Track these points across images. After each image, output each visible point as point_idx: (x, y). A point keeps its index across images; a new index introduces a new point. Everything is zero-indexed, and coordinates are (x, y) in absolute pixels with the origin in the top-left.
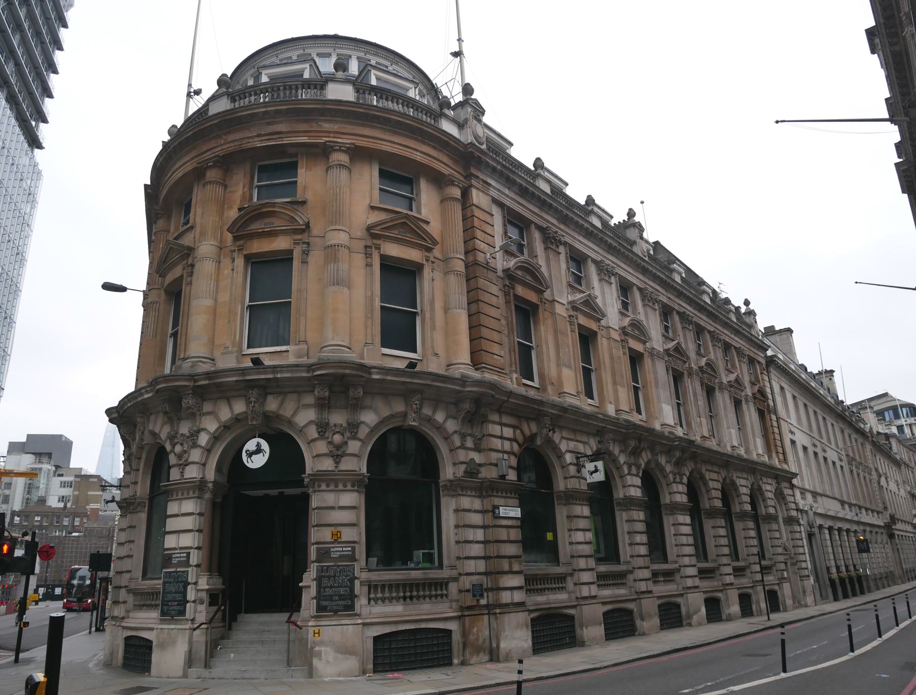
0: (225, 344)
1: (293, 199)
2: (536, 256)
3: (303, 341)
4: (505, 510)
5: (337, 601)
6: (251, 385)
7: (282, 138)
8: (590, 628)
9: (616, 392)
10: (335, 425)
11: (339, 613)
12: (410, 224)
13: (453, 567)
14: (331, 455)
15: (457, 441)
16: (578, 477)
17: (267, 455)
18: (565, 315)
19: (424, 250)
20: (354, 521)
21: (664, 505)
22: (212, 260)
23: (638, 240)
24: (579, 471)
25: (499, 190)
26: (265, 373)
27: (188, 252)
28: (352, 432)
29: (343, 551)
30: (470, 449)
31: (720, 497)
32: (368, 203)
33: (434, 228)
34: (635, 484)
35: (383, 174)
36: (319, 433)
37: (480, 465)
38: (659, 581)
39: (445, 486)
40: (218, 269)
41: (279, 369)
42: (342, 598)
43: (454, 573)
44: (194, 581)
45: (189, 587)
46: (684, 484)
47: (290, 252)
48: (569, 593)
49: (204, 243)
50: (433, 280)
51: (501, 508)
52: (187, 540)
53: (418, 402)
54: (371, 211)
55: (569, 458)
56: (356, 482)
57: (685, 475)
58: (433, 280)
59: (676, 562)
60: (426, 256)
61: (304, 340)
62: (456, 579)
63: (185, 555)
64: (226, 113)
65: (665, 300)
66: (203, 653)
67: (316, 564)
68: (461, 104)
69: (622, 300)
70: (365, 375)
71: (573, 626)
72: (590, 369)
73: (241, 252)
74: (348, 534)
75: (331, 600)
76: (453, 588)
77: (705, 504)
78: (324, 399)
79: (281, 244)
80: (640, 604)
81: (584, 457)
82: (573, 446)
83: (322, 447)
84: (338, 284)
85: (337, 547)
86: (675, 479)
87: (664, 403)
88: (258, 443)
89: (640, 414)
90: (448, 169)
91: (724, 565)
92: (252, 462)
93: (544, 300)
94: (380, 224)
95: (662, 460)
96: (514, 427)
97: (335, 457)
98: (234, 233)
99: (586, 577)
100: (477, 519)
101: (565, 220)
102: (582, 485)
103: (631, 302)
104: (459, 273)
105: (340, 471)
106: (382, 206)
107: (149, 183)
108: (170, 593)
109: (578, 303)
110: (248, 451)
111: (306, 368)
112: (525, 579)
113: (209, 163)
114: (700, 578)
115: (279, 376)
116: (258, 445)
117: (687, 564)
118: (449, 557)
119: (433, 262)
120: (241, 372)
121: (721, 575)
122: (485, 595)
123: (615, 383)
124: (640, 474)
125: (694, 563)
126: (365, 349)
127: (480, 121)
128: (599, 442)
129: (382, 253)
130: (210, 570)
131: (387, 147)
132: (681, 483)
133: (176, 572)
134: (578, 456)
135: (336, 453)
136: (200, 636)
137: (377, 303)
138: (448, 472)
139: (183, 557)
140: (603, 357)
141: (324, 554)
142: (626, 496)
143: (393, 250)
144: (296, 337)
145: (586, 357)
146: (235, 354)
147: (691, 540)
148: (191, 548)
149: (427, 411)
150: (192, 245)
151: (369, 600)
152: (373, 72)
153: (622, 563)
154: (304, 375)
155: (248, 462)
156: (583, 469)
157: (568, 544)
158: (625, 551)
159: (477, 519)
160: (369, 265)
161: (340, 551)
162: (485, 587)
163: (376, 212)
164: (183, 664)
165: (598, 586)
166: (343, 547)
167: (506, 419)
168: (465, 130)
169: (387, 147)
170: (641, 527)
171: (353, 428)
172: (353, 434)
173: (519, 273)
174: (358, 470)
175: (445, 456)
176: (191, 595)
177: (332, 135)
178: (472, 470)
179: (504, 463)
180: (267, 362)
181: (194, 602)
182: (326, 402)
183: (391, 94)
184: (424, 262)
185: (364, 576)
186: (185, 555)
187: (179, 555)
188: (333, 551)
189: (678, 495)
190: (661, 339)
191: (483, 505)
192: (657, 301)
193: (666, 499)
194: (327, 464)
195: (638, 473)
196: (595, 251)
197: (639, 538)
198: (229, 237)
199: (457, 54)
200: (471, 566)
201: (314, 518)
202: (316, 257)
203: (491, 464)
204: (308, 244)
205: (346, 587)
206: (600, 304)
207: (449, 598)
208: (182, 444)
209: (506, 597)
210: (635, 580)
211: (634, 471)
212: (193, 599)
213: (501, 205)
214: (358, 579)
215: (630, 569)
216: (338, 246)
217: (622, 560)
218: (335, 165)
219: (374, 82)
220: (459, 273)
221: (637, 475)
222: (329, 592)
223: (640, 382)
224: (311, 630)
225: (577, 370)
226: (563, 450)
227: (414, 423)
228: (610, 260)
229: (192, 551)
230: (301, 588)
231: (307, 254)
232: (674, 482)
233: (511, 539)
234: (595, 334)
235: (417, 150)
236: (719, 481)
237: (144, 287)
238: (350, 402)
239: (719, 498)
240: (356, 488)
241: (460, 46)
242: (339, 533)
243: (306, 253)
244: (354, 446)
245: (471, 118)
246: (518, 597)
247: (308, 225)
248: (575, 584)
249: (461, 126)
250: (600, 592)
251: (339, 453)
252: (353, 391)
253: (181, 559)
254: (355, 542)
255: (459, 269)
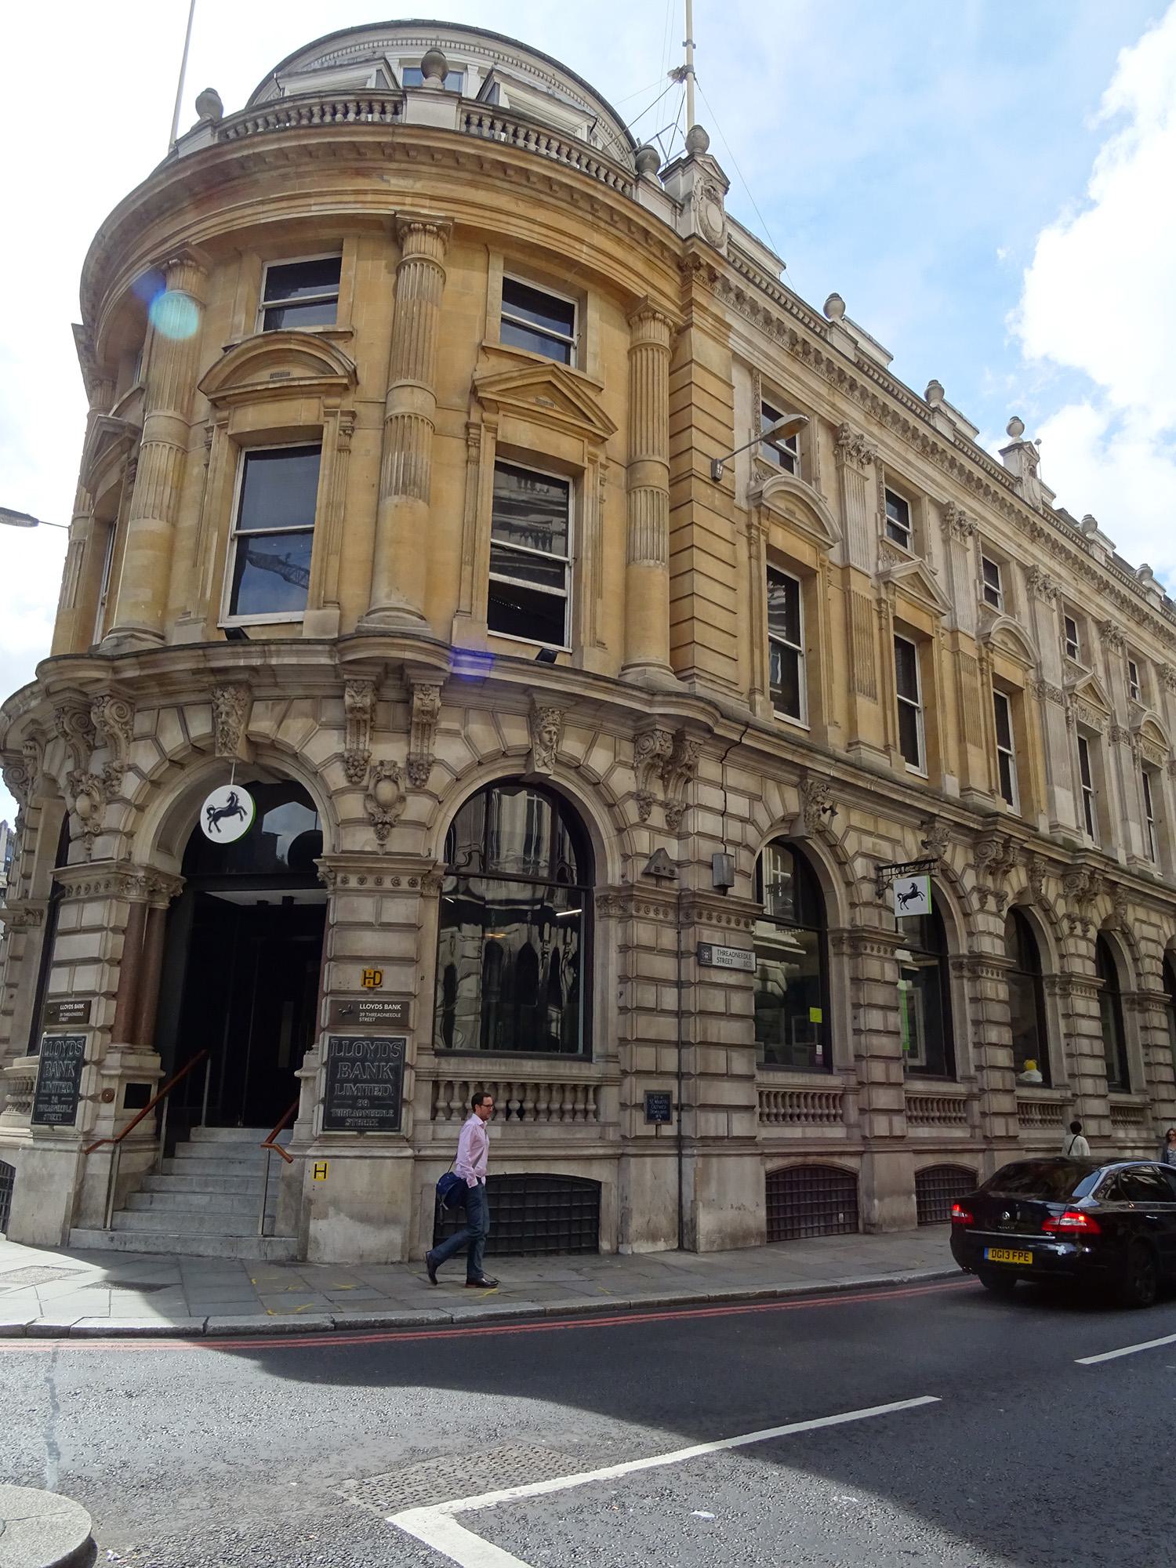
0: (185, 607)
1: (330, 328)
2: (817, 480)
3: (334, 602)
4: (724, 953)
5: (367, 1108)
6: (223, 678)
7: (310, 205)
8: (887, 1200)
9: (963, 755)
10: (382, 763)
11: (369, 1133)
12: (560, 386)
13: (613, 1058)
14: (371, 821)
15: (632, 810)
16: (879, 906)
17: (248, 819)
18: (869, 597)
19: (586, 441)
20: (412, 954)
21: (1048, 976)
22: (168, 446)
23: (1025, 476)
24: (880, 894)
25: (749, 342)
26: (247, 655)
27: (133, 437)
28: (416, 779)
29: (383, 1011)
30: (659, 831)
31: (1161, 973)
32: (477, 341)
33: (613, 403)
34: (992, 930)
35: (513, 293)
36: (350, 777)
37: (679, 864)
38: (1032, 1120)
39: (605, 899)
40: (182, 467)
41: (273, 648)
42: (376, 1102)
43: (613, 1069)
44: (95, 1058)
45: (85, 1070)
46: (1090, 940)
47: (317, 431)
48: (849, 1126)
49: (154, 413)
50: (602, 501)
51: (714, 949)
52: (87, 979)
53: (553, 729)
54: (482, 357)
55: (860, 867)
56: (424, 877)
57: (1092, 923)
58: (602, 501)
59: (1066, 1087)
60: (590, 453)
61: (334, 599)
62: (617, 1082)
63: (82, 1006)
64: (210, 153)
65: (1071, 593)
66: (102, 1200)
67: (328, 1035)
68: (680, 165)
69: (987, 588)
70: (444, 666)
71: (854, 1192)
72: (914, 708)
73: (224, 431)
74: (395, 979)
75: (353, 1107)
76: (610, 1098)
77: (1129, 982)
78: (362, 710)
79: (301, 412)
80: (992, 1158)
81: (891, 867)
82: (871, 846)
83: (353, 806)
84: (405, 492)
85: (373, 1003)
86: (1072, 929)
87: (1060, 785)
88: (232, 793)
89: (1010, 802)
90: (645, 286)
91: (1164, 1101)
92: (219, 830)
93: (827, 564)
94: (499, 382)
95: (1051, 889)
96: (755, 798)
97: (380, 826)
98: (212, 393)
99: (884, 1098)
100: (665, 967)
101: (881, 414)
102: (884, 922)
103: (1005, 592)
104: (655, 490)
105: (387, 854)
106: (504, 348)
107: (81, 323)
108: (53, 1078)
109: (897, 576)
110: (213, 809)
111: (327, 648)
112: (761, 1094)
113: (172, 259)
114: (1114, 1122)
115: (274, 661)
116: (233, 798)
117: (1090, 1093)
118: (604, 1037)
119: (605, 467)
120: (200, 652)
121: (1155, 1119)
122: (675, 1115)
123: (962, 738)
124: (1004, 913)
125: (1103, 1090)
126: (455, 623)
127: (718, 202)
128: (923, 843)
129: (499, 439)
130: (132, 1038)
131: (518, 230)
132: (1084, 938)
133: (65, 1039)
134: (880, 866)
135: (380, 817)
136: (100, 1165)
137: (486, 537)
138: (612, 871)
139: (79, 1010)
140: (942, 687)
141: (347, 1014)
142: (973, 952)
143: (522, 434)
144: (319, 595)
145: (908, 684)
146: (203, 624)
147: (1098, 1047)
148: (93, 994)
149: (572, 746)
150: (139, 424)
151: (435, 1111)
152: (503, 87)
153: (958, 1079)
154: (324, 660)
155: (210, 831)
156: (888, 891)
157: (850, 1032)
158: (966, 1056)
159: (665, 967)
160: (472, 461)
161: (378, 1011)
162: (675, 1101)
163: (494, 360)
164: (62, 1218)
165: (910, 1118)
166: (383, 1003)
167: (734, 777)
168: (685, 216)
169: (519, 230)
170: (999, 1012)
171: (418, 769)
172: (418, 783)
173: (782, 504)
174: (425, 853)
175: (606, 842)
176: (88, 1083)
177: (408, 200)
178: (660, 871)
179: (725, 862)
180: (252, 635)
181: (93, 1098)
182: (367, 717)
183: (535, 128)
184: (586, 464)
185: (427, 1062)
186: (82, 1006)
187: (71, 1007)
188: (363, 1011)
189: (1078, 961)
190: (1059, 668)
191: (679, 941)
192: (1055, 595)
193: (1052, 965)
194: (363, 839)
195: (1000, 911)
196: (938, 485)
197: (993, 1034)
198: (203, 404)
199: (682, 74)
200: (645, 1058)
201: (333, 943)
202: (366, 440)
203: (700, 862)
204: (353, 415)
205: (386, 1082)
206: (942, 586)
207: (602, 1119)
208: (88, 794)
209: (714, 1124)
210: (984, 1114)
211: (991, 904)
212: (91, 1093)
213: (751, 369)
214: (412, 1067)
215: (976, 1090)
216: (410, 417)
217: (959, 1073)
218: (413, 260)
219: (504, 103)
220: (655, 490)
221: (998, 914)
222: (351, 1089)
223: (1012, 746)
224: (310, 1165)
225: (888, 705)
226: (851, 853)
227: (543, 770)
228: (969, 505)
229: (94, 1000)
230: (298, 1080)
231: (350, 436)
232: (1071, 934)
233: (733, 1011)
234: (926, 639)
235: (581, 241)
236: (1160, 944)
237: (68, 523)
238: (415, 719)
239: (1158, 975)
240: (418, 888)
241: (689, 56)
242: (378, 975)
243: (348, 432)
244: (417, 807)
245: (699, 192)
246: (741, 1126)
247: (353, 375)
248: (862, 1111)
249: (679, 206)
250: (910, 1129)
251: (387, 819)
252: (422, 696)
253: (75, 1014)
254: (410, 994)
255: (656, 483)
